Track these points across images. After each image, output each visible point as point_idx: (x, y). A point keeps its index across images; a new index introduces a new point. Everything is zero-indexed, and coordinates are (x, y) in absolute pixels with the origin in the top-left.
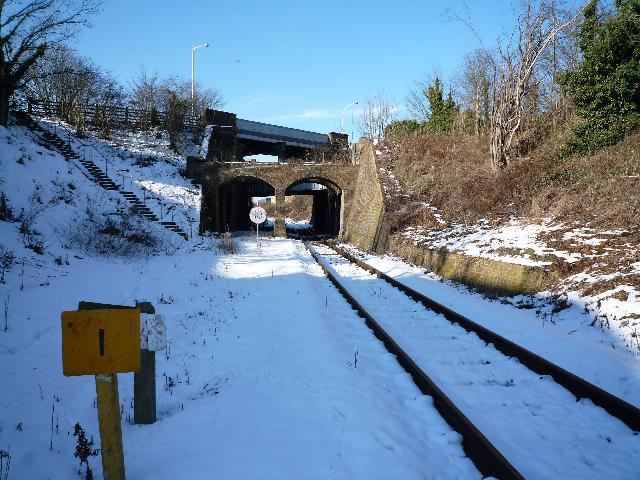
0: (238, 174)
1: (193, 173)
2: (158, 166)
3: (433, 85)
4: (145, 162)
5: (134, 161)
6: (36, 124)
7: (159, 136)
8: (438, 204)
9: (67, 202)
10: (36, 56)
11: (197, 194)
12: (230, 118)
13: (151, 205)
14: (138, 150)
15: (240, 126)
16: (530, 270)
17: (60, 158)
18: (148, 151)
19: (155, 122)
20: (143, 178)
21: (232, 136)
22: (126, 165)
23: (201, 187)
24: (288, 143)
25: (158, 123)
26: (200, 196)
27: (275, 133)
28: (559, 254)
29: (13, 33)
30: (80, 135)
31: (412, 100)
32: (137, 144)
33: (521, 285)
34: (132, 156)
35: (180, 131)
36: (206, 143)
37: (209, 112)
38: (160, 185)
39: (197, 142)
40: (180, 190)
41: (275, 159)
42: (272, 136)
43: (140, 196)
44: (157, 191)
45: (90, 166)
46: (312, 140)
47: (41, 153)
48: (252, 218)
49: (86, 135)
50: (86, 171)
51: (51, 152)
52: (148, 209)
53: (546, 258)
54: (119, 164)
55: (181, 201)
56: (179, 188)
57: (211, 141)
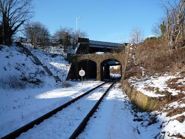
0: (89, 60)
1: (69, 59)
2: (58, 57)
3: (162, 24)
4: (54, 56)
5: (50, 56)
6: (22, 46)
7: (61, 47)
8: (170, 66)
9: (18, 70)
10: (20, 24)
11: (69, 66)
12: (87, 40)
13: (52, 70)
14: (53, 53)
15: (90, 43)
16: (150, 99)
17: (24, 56)
18: (56, 52)
19: (61, 43)
20: (51, 61)
21: (87, 45)
22: (47, 57)
23: (71, 63)
24: (107, 48)
25: (62, 43)
26: (70, 67)
27: (100, 44)
28: (170, 90)
29: (11, 17)
30: (35, 48)
31: (154, 29)
32: (53, 50)
33: (147, 106)
34: (50, 54)
35: (68, 45)
36: (76, 49)
37: (79, 38)
38: (57, 63)
39: (74, 49)
40: (63, 65)
41: (103, 53)
42: (101, 46)
43: (49, 67)
44: (55, 65)
45: (36, 58)
46: (117, 46)
47: (18, 54)
48: (80, 74)
49: (37, 48)
50: (33, 60)
51: (21, 54)
52: (51, 72)
53: (163, 93)
54: (45, 57)
55: (63, 69)
56: (63, 64)
57: (78, 49)
